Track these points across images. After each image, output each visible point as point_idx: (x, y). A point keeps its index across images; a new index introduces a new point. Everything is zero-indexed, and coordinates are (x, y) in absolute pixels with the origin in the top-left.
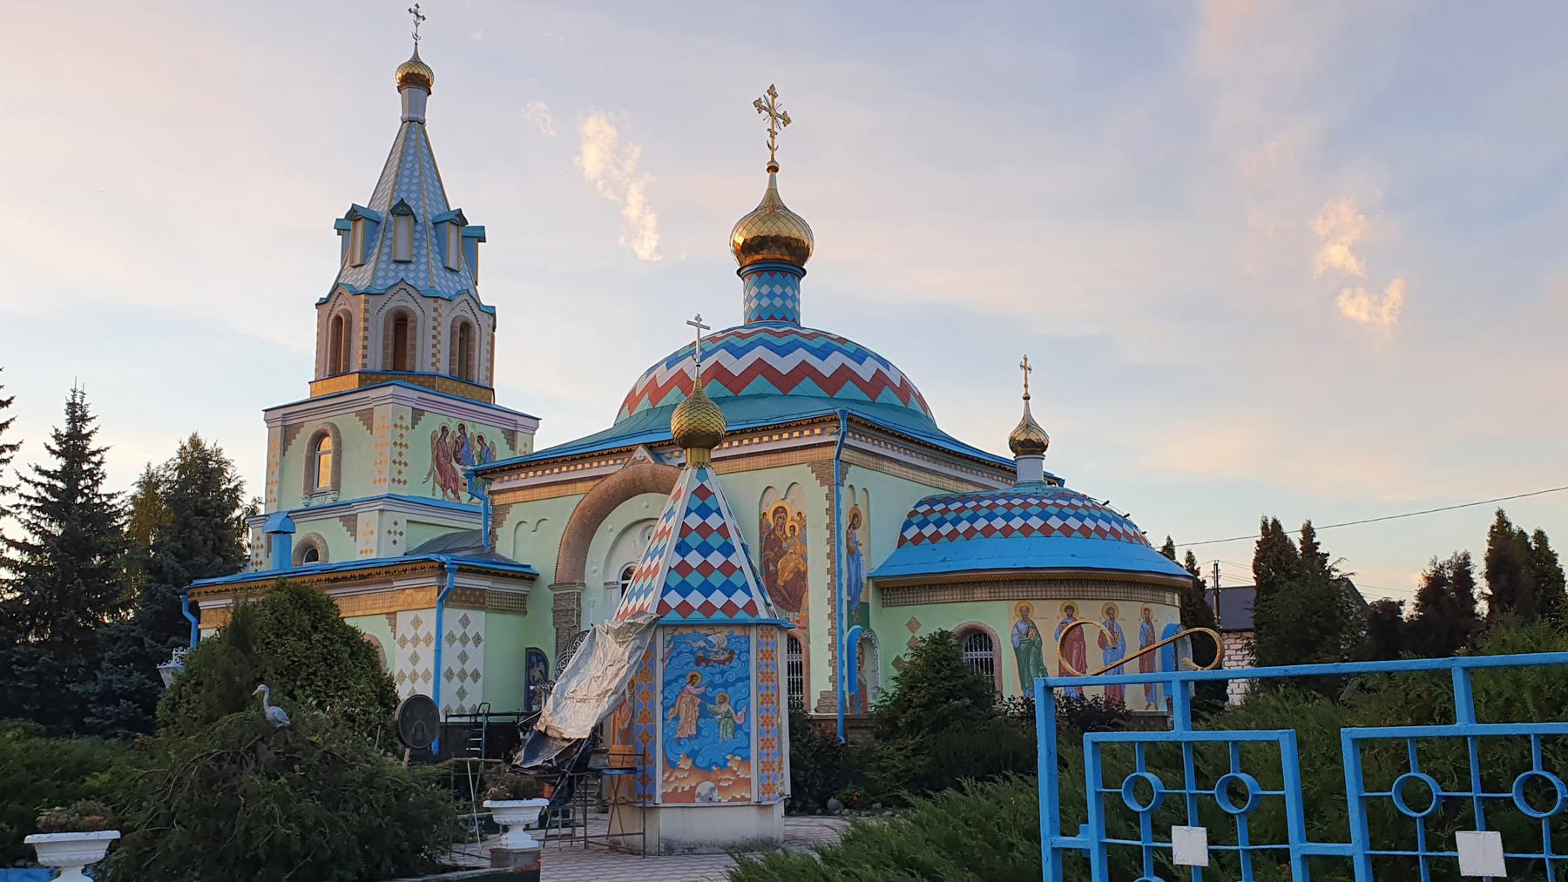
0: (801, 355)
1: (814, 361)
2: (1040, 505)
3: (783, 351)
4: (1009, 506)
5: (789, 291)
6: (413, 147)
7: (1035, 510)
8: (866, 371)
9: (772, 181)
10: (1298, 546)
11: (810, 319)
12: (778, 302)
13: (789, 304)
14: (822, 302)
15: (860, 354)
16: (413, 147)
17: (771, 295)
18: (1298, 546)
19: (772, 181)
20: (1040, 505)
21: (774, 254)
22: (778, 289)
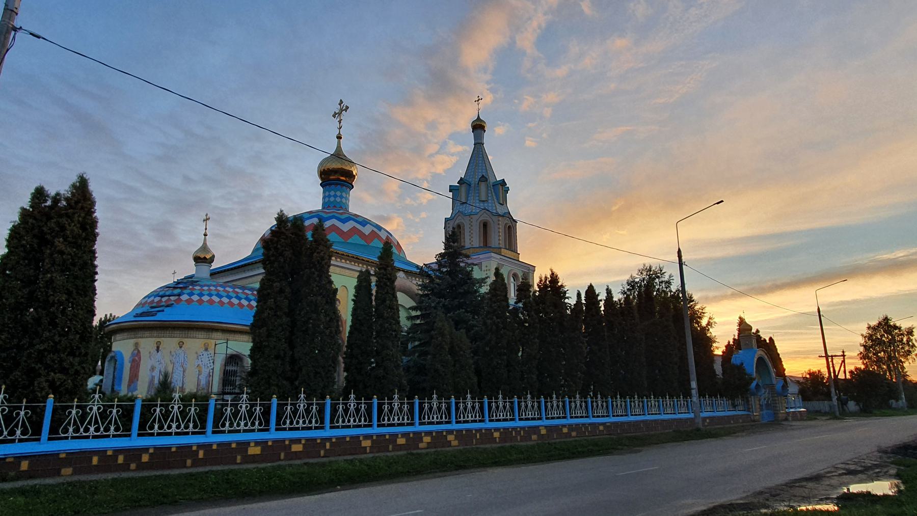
0: (350, 225)
1: (359, 226)
2: (216, 290)
3: (344, 221)
4: (210, 290)
5: (344, 194)
6: (479, 155)
7: (214, 293)
8: (367, 230)
9: (339, 143)
10: (346, 307)
11: (353, 209)
12: (332, 199)
13: (344, 201)
14: (361, 201)
15: (365, 222)
16: (479, 155)
17: (335, 196)
18: (346, 307)
19: (339, 143)
20: (216, 290)
21: (337, 176)
22: (338, 193)
